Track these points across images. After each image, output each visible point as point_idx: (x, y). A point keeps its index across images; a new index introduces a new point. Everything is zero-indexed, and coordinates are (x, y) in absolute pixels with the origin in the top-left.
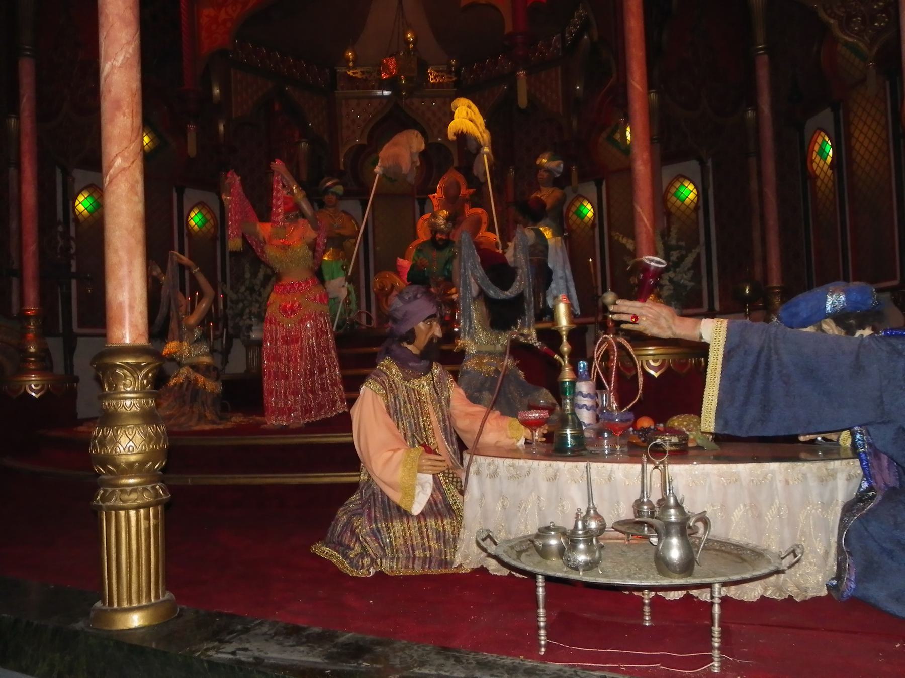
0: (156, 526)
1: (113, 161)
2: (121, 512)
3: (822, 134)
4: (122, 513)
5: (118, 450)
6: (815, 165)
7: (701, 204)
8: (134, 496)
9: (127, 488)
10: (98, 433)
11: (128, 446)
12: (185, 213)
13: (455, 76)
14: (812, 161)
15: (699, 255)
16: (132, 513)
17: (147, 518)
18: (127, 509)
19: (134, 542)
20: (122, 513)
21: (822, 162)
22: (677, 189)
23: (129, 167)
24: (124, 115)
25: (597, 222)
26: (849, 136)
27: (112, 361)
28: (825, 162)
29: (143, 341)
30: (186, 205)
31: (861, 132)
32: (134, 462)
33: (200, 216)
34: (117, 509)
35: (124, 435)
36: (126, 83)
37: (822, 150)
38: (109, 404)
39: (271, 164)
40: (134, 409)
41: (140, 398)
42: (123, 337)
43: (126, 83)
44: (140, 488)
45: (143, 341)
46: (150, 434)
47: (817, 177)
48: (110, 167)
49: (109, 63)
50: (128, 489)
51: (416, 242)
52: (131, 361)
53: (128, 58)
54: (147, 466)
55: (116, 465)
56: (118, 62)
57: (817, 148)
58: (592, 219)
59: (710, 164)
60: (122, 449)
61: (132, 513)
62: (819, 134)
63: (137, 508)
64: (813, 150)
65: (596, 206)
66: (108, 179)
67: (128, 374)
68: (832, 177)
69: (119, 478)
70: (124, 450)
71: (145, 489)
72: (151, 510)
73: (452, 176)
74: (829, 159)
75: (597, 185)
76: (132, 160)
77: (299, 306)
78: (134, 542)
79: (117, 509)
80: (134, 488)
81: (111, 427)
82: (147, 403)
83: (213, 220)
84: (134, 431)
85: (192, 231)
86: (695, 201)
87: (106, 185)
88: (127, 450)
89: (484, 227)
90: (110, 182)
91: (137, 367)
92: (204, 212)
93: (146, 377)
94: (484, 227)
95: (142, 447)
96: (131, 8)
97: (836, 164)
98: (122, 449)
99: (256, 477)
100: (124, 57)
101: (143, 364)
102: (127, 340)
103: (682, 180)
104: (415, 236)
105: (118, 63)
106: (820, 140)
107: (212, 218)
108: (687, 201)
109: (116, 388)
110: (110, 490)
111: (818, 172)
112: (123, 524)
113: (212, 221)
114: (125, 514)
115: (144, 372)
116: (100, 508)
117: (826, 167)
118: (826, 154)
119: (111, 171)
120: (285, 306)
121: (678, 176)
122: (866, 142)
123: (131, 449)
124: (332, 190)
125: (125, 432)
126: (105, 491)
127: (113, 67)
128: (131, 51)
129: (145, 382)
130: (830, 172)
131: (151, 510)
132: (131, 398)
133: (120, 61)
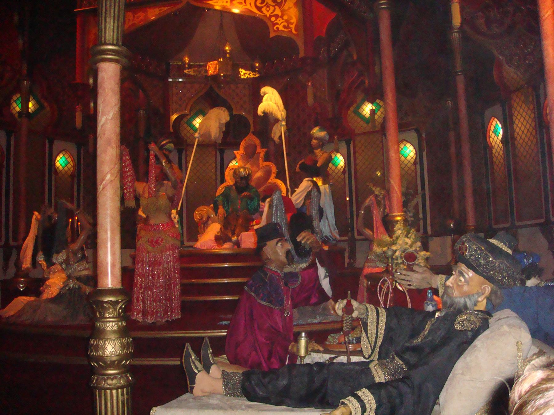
0: (127, 399)
1: (105, 176)
2: (108, 391)
3: (496, 119)
4: (108, 391)
5: (106, 353)
6: (491, 139)
7: (418, 160)
8: (115, 381)
9: (111, 376)
10: (94, 343)
11: (112, 351)
12: (54, 156)
13: (258, 73)
14: (490, 137)
15: (417, 203)
16: (114, 392)
17: (123, 394)
18: (111, 389)
19: (115, 409)
20: (108, 391)
21: (496, 138)
22: (402, 149)
23: (114, 179)
24: (112, 148)
25: (347, 169)
26: (512, 123)
27: (102, 299)
28: (498, 138)
29: (119, 286)
30: (54, 149)
31: (519, 113)
32: (115, 361)
33: (64, 159)
34: (106, 389)
35: (109, 345)
36: (114, 129)
37: (495, 132)
38: (99, 325)
39: (148, 146)
40: (114, 328)
41: (118, 321)
42: (108, 285)
43: (114, 129)
44: (118, 376)
45: (119, 286)
46: (124, 344)
47: (493, 147)
48: (103, 180)
49: (105, 117)
50: (112, 377)
51: (224, 185)
52: (112, 299)
53: (115, 114)
54: (122, 363)
55: (105, 362)
56: (110, 116)
57: (492, 128)
58: (344, 167)
59: (424, 135)
60: (108, 353)
61: (114, 392)
62: (494, 119)
63: (117, 389)
64: (490, 130)
65: (346, 158)
66: (101, 187)
67: (111, 306)
68: (503, 156)
69: (106, 370)
70: (110, 353)
71: (121, 377)
72: (125, 390)
73: (251, 139)
74: (500, 137)
75: (346, 144)
76: (116, 175)
77: (162, 240)
78: (115, 409)
79: (106, 389)
80: (114, 376)
81: (100, 339)
82: (122, 324)
83: (73, 162)
84: (115, 342)
85: (58, 170)
86: (414, 157)
87: (100, 190)
88: (111, 354)
89: (273, 176)
90: (103, 188)
91: (116, 303)
92: (67, 156)
93: (121, 308)
94: (273, 176)
95: (120, 351)
96: (118, 84)
97: (505, 140)
98: (108, 353)
99: (144, 361)
100: (114, 113)
101: (120, 301)
102: (110, 286)
103: (405, 142)
104: (223, 180)
105: (109, 118)
106: (494, 123)
107: (72, 160)
108: (409, 158)
109: (104, 315)
110: (101, 377)
111: (493, 144)
112: (109, 398)
113: (71, 163)
114: (110, 393)
115: (120, 305)
116: (96, 388)
117: (498, 142)
118: (498, 133)
119: (104, 182)
120: (152, 240)
121: (403, 139)
122: (523, 128)
123: (113, 353)
124: (165, 147)
125: (110, 342)
126: (98, 378)
127: (107, 119)
128: (117, 110)
129: (120, 311)
130: (501, 145)
131: (125, 390)
132: (113, 322)
133: (111, 116)
